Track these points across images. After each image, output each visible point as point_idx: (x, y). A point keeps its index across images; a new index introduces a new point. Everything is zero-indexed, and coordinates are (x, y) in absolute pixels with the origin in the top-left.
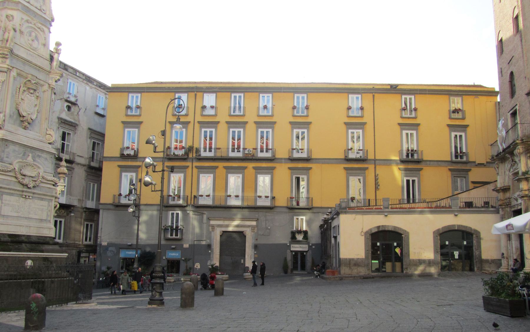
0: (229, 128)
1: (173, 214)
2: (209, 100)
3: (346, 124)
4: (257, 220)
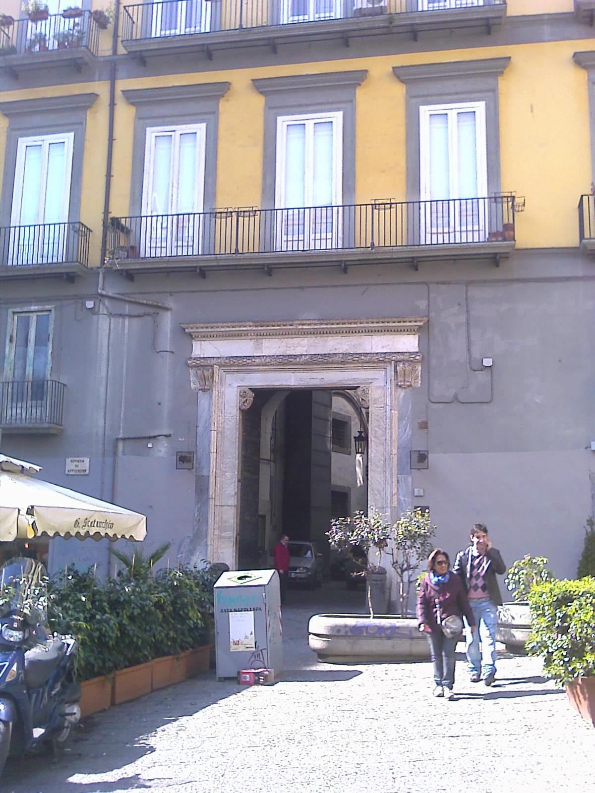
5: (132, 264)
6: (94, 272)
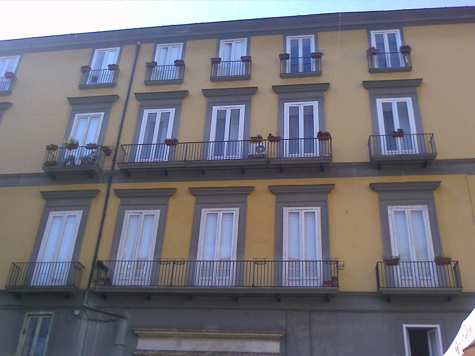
3: (366, 85)
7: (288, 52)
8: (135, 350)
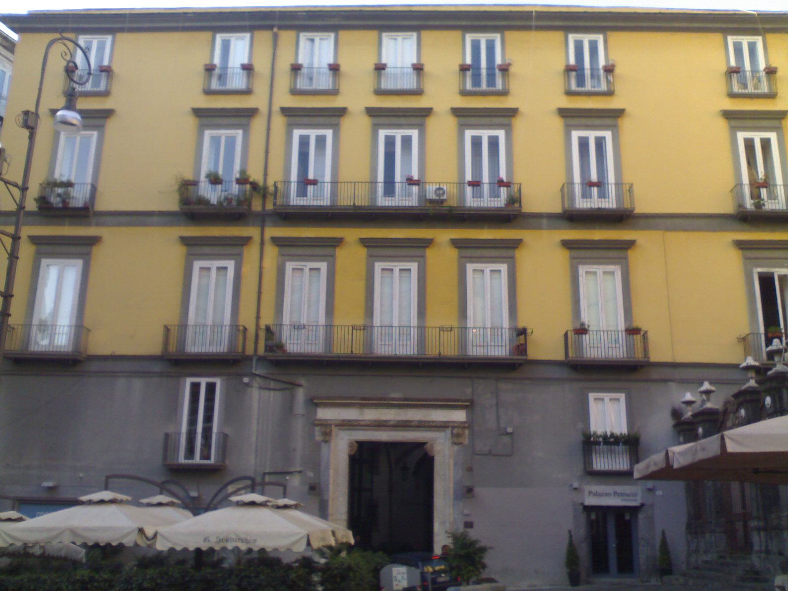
0: (376, 127)
1: (195, 387)
2: (318, 51)
4: (469, 406)
5: (278, 355)
6: (249, 358)
7: (469, 61)
8: (317, 420)
